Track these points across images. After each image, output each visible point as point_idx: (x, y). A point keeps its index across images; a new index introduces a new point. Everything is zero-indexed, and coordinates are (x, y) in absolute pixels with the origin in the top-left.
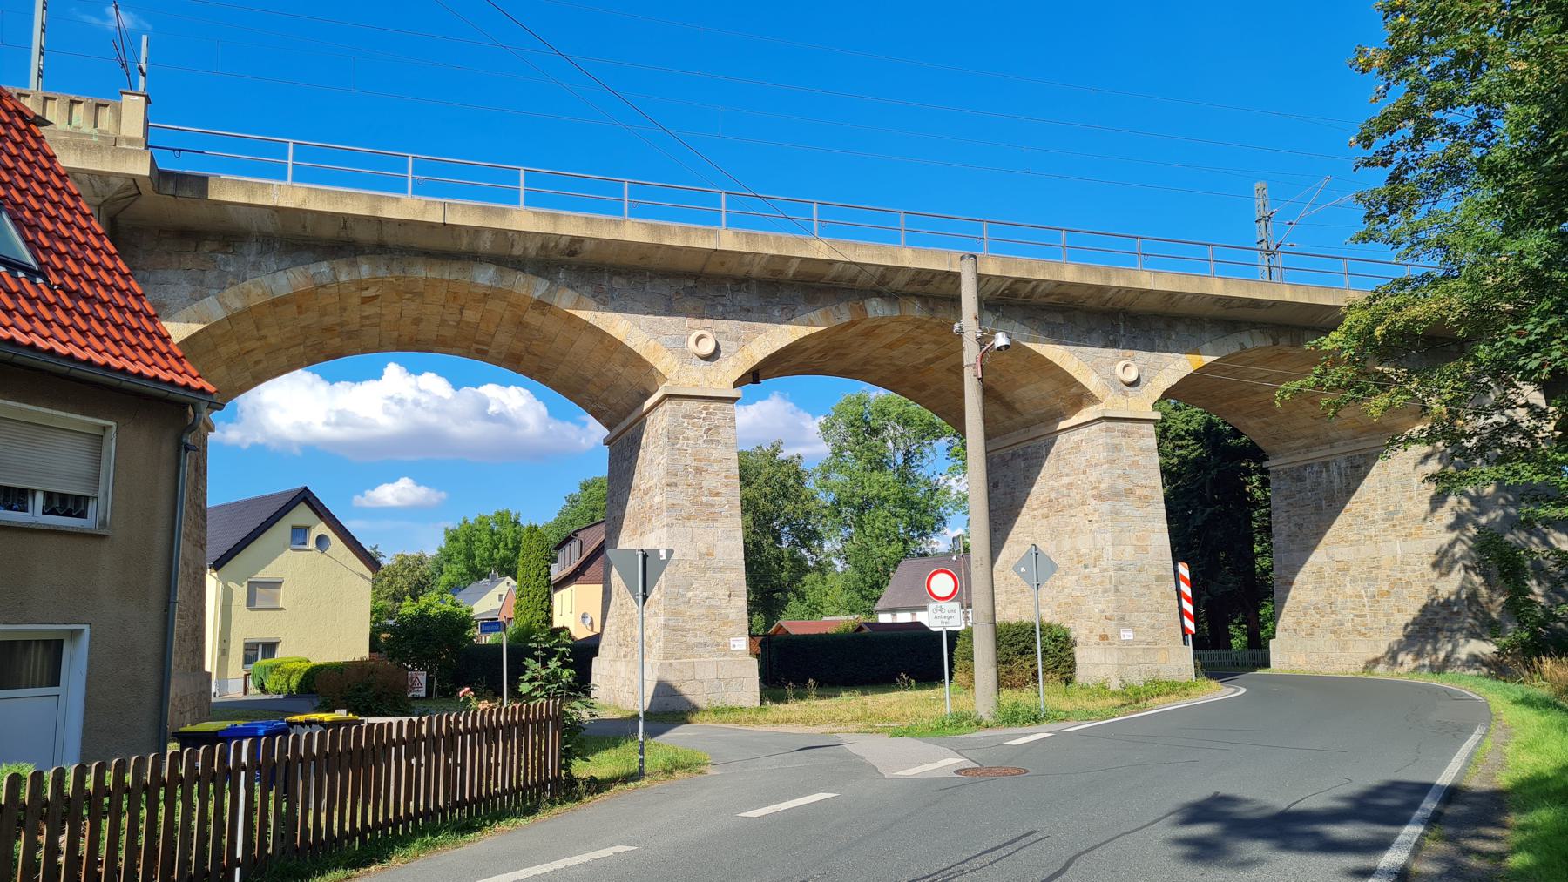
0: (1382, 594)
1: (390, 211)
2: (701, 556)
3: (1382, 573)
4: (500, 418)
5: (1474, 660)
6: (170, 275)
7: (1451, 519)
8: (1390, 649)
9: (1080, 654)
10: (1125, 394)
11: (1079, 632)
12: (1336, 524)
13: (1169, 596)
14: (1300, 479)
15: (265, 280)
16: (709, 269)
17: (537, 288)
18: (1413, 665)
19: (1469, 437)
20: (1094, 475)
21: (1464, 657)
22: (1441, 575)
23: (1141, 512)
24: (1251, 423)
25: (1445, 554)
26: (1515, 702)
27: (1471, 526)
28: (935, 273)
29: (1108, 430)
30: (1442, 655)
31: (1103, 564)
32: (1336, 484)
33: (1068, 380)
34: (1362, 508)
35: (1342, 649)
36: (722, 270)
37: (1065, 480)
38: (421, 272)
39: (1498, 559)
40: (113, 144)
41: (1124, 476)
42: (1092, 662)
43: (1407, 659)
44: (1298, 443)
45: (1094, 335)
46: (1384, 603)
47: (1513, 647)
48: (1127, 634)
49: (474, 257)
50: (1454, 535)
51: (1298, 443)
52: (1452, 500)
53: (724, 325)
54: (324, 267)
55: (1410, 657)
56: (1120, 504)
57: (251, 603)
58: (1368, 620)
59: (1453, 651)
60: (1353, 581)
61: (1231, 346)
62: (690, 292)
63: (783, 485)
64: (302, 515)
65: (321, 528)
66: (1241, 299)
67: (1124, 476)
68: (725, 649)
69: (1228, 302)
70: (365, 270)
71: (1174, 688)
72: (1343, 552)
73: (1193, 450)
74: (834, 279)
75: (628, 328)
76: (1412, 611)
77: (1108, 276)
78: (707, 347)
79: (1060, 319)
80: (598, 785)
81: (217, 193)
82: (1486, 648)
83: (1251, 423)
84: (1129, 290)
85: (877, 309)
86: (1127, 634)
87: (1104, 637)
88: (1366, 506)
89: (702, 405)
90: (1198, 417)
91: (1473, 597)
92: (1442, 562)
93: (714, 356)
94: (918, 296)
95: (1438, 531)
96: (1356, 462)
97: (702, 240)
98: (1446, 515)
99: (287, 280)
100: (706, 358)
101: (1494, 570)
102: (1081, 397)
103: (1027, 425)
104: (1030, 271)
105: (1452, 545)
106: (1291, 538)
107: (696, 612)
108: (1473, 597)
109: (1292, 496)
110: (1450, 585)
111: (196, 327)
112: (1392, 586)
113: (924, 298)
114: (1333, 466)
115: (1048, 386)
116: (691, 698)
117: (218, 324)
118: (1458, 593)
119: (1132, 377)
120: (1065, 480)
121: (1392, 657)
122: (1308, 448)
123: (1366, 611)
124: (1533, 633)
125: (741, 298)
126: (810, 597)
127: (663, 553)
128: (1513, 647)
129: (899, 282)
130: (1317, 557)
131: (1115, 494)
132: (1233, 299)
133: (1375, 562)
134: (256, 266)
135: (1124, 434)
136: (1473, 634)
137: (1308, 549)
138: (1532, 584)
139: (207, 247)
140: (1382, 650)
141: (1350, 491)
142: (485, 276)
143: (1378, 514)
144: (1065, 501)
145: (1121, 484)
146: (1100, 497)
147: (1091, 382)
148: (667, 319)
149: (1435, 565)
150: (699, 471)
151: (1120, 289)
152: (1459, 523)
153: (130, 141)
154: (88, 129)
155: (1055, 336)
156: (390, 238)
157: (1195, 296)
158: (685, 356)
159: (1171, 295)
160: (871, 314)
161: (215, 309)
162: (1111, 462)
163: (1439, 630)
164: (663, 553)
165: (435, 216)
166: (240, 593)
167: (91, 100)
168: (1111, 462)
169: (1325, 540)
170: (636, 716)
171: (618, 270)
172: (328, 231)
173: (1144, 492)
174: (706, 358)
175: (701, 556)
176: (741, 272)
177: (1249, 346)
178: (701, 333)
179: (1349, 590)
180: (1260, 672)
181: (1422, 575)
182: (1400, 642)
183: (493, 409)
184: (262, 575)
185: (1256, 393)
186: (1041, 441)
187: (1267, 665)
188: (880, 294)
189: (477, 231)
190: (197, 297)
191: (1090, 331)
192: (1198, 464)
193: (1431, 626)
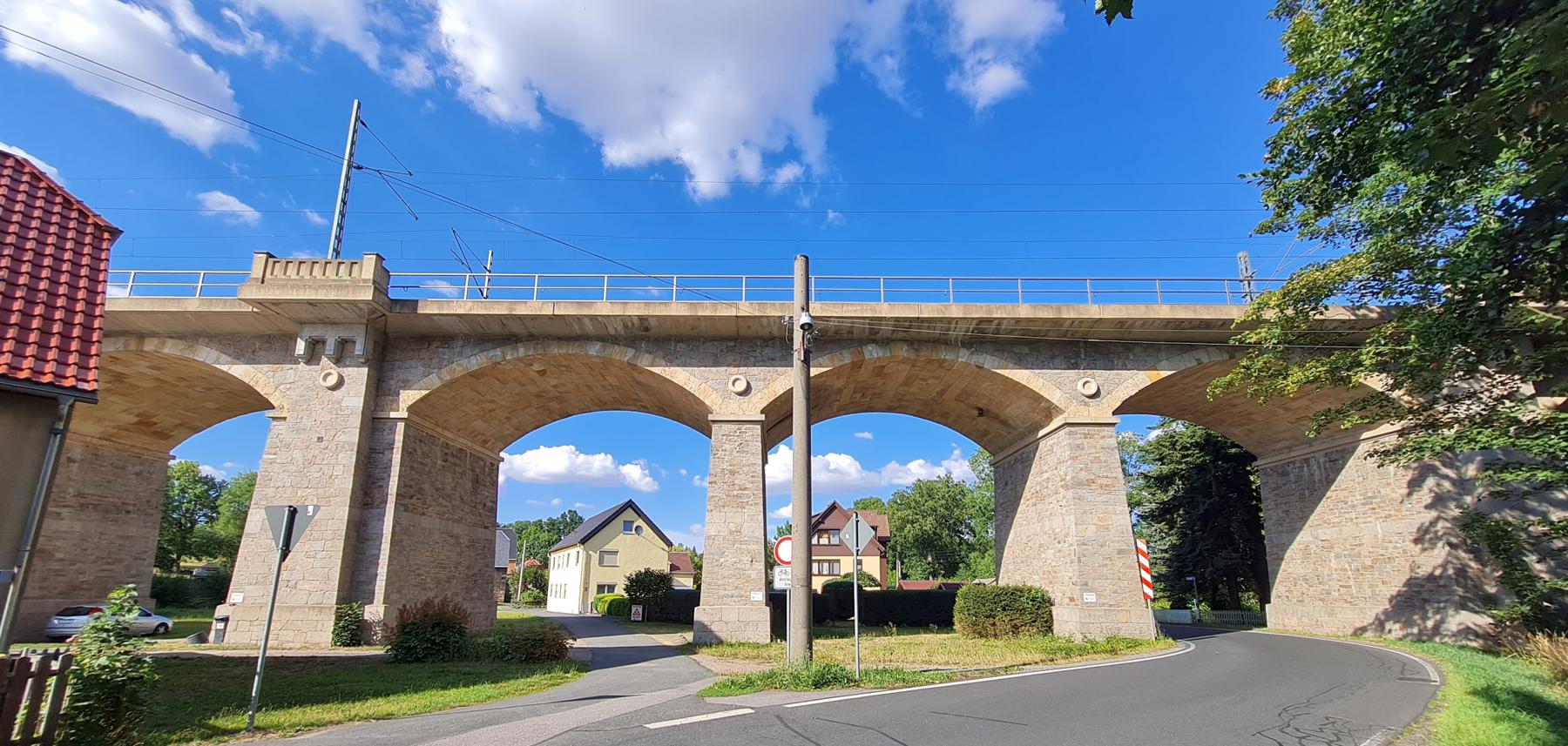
0: (1365, 568)
1: (521, 310)
2: (731, 533)
3: (1364, 550)
4: (836, 471)
5: (1467, 632)
6: (413, 363)
7: (1428, 500)
8: (1377, 618)
9: (1056, 611)
10: (1086, 404)
11: (1055, 593)
12: (1318, 509)
13: (1132, 567)
14: (1285, 474)
15: (464, 362)
16: (743, 332)
17: (623, 355)
18: (1400, 634)
19: (1449, 426)
20: (1063, 469)
21: (1454, 628)
22: (1424, 550)
23: (1104, 498)
24: (1236, 431)
25: (1427, 531)
26: (1475, 693)
27: (1452, 505)
28: (911, 320)
29: (1070, 433)
30: (1430, 624)
31: (1069, 539)
32: (1316, 477)
33: (1036, 398)
34: (1342, 495)
35: (1330, 615)
36: (751, 333)
37: (1046, 476)
38: (555, 350)
39: (1487, 536)
40: (357, 285)
41: (1086, 469)
42: (1066, 620)
43: (1395, 629)
44: (1280, 445)
45: (1057, 361)
46: (1368, 575)
47: (1512, 620)
48: (1091, 598)
49: (585, 338)
50: (1434, 514)
51: (1280, 445)
52: (1431, 482)
53: (755, 370)
54: (498, 352)
55: (1397, 626)
56: (1081, 492)
57: (601, 563)
58: (1354, 590)
59: (1442, 621)
60: (1337, 557)
61: (1188, 362)
62: (731, 350)
63: (954, 499)
64: (629, 515)
65: (640, 522)
66: (1191, 321)
67: (1086, 469)
68: (746, 600)
69: (1179, 323)
70: (521, 351)
71: (1134, 644)
72: (1327, 533)
73: (1196, 457)
74: (836, 332)
75: (686, 377)
76: (1396, 585)
77: (1059, 310)
78: (741, 386)
79: (1026, 350)
80: (226, 732)
81: (426, 308)
82: (1483, 621)
83: (1236, 431)
84: (1082, 321)
85: (872, 352)
86: (1091, 598)
87: (1072, 599)
88: (1345, 493)
89: (734, 427)
90: (1199, 433)
91: (1462, 572)
92: (1423, 537)
93: (746, 392)
94: (905, 341)
95: (1418, 512)
96: (1334, 457)
97: (725, 310)
98: (1425, 495)
99: (477, 361)
100: (740, 394)
101: (1483, 546)
102: (1050, 411)
103: (1022, 437)
104: (990, 312)
105: (1433, 523)
106: (1279, 522)
107: (726, 573)
108: (1462, 572)
109: (1279, 488)
110: (1433, 560)
111: (425, 392)
112: (1375, 561)
113: (910, 342)
114: (1313, 462)
115: (1025, 403)
116: (719, 634)
117: (437, 390)
118: (1444, 566)
119: (1093, 390)
120: (1046, 476)
121: (1380, 625)
122: (1289, 448)
123: (1351, 583)
124: (1536, 606)
125: (768, 351)
126: (973, 566)
127: (311, 509)
128: (1512, 620)
129: (886, 328)
130: (1303, 537)
131: (1079, 484)
132: (1182, 321)
133: (1359, 539)
134: (460, 354)
135: (1086, 436)
136: (1462, 606)
137: (1295, 531)
138: (1531, 558)
139: (435, 344)
140: (1369, 618)
141: (1329, 481)
142: (594, 349)
143: (1358, 498)
144: (1045, 492)
145: (1083, 476)
146: (1066, 487)
147: (1055, 396)
148: (714, 369)
149: (1416, 541)
150: (732, 473)
151: (1073, 321)
152: (1439, 501)
153: (365, 281)
154: (346, 277)
155: (1021, 363)
156: (517, 329)
157: (1145, 321)
158: (726, 396)
159: (1121, 322)
160: (867, 356)
161: (434, 381)
162: (1074, 458)
163: (1426, 601)
164: (311, 509)
165: (547, 310)
166: (595, 557)
167: (349, 262)
168: (1074, 458)
169: (1309, 523)
170: (250, 662)
171: (680, 339)
172: (497, 329)
173: (1104, 481)
174: (740, 394)
175: (731, 533)
176: (765, 332)
177: (1205, 360)
178: (739, 376)
179: (1334, 564)
180: (1256, 631)
181: (1405, 551)
182: (1385, 612)
183: (832, 467)
184: (606, 548)
185: (1233, 406)
186: (1030, 448)
187: (1264, 625)
188: (874, 341)
189: (579, 318)
190: (425, 376)
191: (1053, 358)
192: (1200, 468)
193: (1416, 599)
